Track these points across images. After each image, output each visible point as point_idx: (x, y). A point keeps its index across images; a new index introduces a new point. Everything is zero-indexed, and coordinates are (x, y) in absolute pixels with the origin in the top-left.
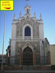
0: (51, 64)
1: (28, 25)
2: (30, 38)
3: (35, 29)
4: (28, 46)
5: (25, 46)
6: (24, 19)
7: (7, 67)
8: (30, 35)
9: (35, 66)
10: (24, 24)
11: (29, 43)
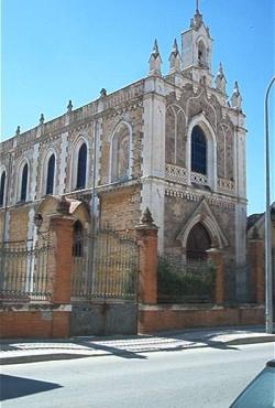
1: (200, 120)
4: (202, 218)
5: (195, 220)
6: (191, 88)
8: (204, 171)
10: (192, 116)
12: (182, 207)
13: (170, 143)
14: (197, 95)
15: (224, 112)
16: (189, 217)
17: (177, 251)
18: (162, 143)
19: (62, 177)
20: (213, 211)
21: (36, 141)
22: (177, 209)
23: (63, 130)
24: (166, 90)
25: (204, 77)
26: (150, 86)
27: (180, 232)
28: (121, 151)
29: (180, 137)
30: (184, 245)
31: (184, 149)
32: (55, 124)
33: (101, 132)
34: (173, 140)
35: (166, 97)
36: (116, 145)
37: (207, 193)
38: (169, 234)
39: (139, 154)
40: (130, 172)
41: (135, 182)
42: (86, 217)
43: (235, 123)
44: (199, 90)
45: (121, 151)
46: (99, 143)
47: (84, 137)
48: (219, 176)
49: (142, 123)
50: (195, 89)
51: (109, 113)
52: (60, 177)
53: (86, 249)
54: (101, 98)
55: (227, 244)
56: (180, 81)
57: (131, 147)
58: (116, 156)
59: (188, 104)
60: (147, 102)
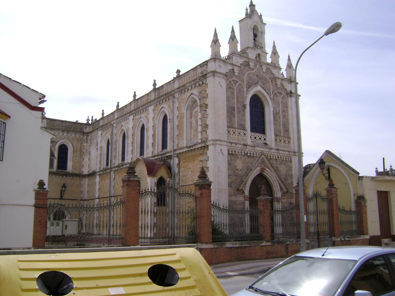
0: (367, 234)
1: (257, 89)
2: (262, 139)
3: (279, 113)
4: (263, 170)
5: (256, 172)
6: (248, 65)
7: (269, 248)
8: (263, 132)
9: (339, 239)
10: (249, 86)
11: (264, 158)
12: (243, 162)
13: (230, 111)
14: (253, 69)
15: (279, 82)
16: (249, 170)
17: (240, 199)
18: (223, 111)
19: (151, 141)
20: (271, 164)
21: (130, 113)
22: (239, 164)
23: (149, 103)
24: (225, 69)
25: (259, 55)
26: (211, 67)
27: (243, 182)
28: (193, 120)
29: (240, 105)
30: (247, 193)
31: (244, 115)
32: (144, 99)
33: (177, 105)
34: (234, 108)
35: (226, 75)
36: (189, 116)
37: (265, 150)
38: (233, 185)
39: (205, 121)
40: (200, 136)
41: (203, 145)
42: (168, 175)
43: (289, 89)
44: (256, 65)
45: (193, 120)
46: (176, 113)
47: (166, 108)
48: (276, 135)
49: (206, 97)
50: (252, 64)
51: (182, 89)
52: (149, 141)
53: (169, 200)
54: (177, 77)
55: (285, 191)
56: (237, 61)
57: (200, 116)
58: (189, 124)
59: (245, 78)
60: (210, 80)
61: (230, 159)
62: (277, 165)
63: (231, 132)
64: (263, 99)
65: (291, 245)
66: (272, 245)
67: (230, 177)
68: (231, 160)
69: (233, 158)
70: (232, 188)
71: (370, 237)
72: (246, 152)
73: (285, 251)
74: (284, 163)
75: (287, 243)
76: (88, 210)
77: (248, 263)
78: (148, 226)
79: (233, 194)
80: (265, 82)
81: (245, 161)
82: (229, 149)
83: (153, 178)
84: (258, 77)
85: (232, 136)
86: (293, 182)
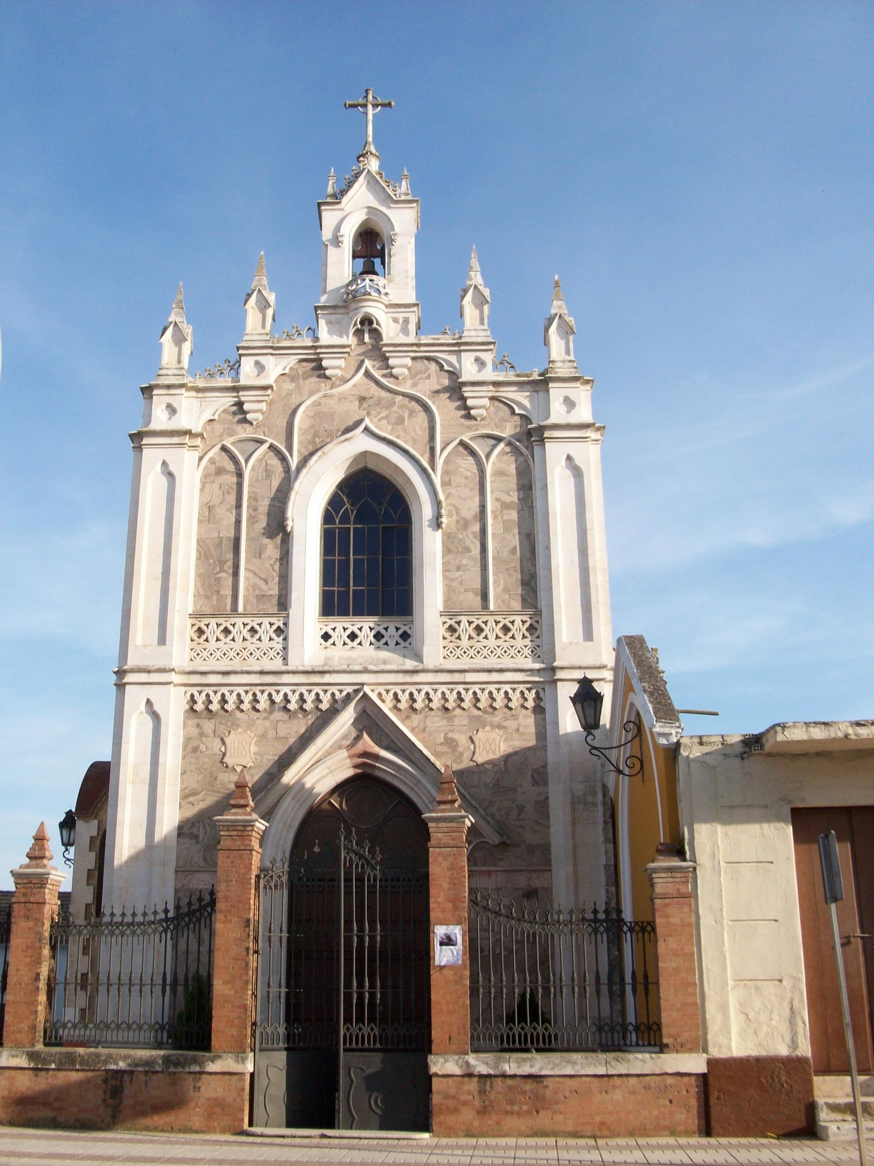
61: (195, 731)
62: (450, 735)
63: (213, 630)
64: (398, 481)
65: (142, 1078)
66: (33, 1069)
67: (191, 799)
68: (202, 734)
69: (208, 726)
70: (197, 842)
71: (712, 1063)
72: (278, 698)
73: (104, 1101)
74: (497, 719)
75: (113, 1067)
76: (128, 932)
77: (75, 1139)
78: (634, 990)
79: (202, 863)
80: (406, 415)
81: (271, 734)
82: (192, 696)
83: (87, 822)
84: (365, 405)
85: (212, 645)
86: (547, 798)
